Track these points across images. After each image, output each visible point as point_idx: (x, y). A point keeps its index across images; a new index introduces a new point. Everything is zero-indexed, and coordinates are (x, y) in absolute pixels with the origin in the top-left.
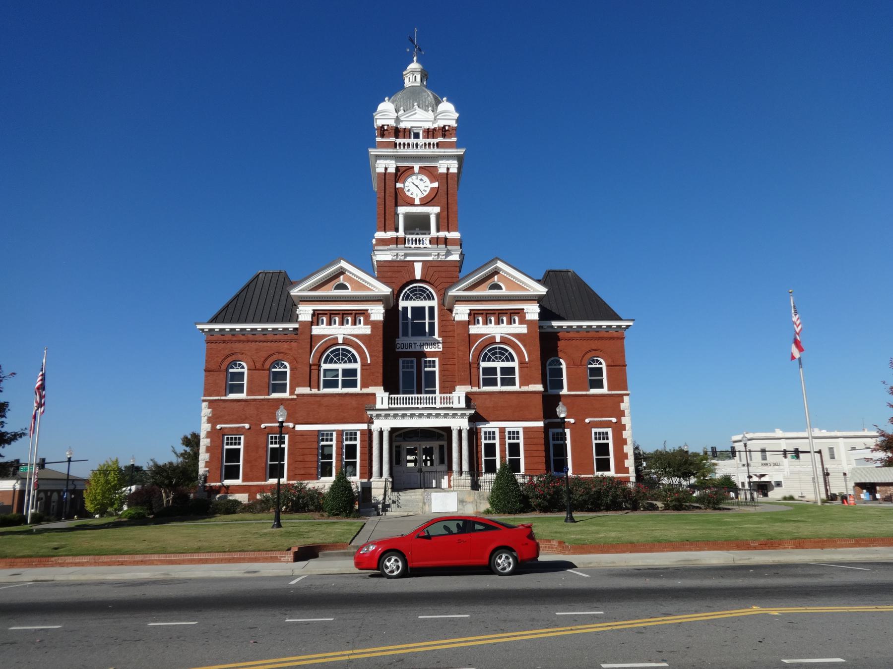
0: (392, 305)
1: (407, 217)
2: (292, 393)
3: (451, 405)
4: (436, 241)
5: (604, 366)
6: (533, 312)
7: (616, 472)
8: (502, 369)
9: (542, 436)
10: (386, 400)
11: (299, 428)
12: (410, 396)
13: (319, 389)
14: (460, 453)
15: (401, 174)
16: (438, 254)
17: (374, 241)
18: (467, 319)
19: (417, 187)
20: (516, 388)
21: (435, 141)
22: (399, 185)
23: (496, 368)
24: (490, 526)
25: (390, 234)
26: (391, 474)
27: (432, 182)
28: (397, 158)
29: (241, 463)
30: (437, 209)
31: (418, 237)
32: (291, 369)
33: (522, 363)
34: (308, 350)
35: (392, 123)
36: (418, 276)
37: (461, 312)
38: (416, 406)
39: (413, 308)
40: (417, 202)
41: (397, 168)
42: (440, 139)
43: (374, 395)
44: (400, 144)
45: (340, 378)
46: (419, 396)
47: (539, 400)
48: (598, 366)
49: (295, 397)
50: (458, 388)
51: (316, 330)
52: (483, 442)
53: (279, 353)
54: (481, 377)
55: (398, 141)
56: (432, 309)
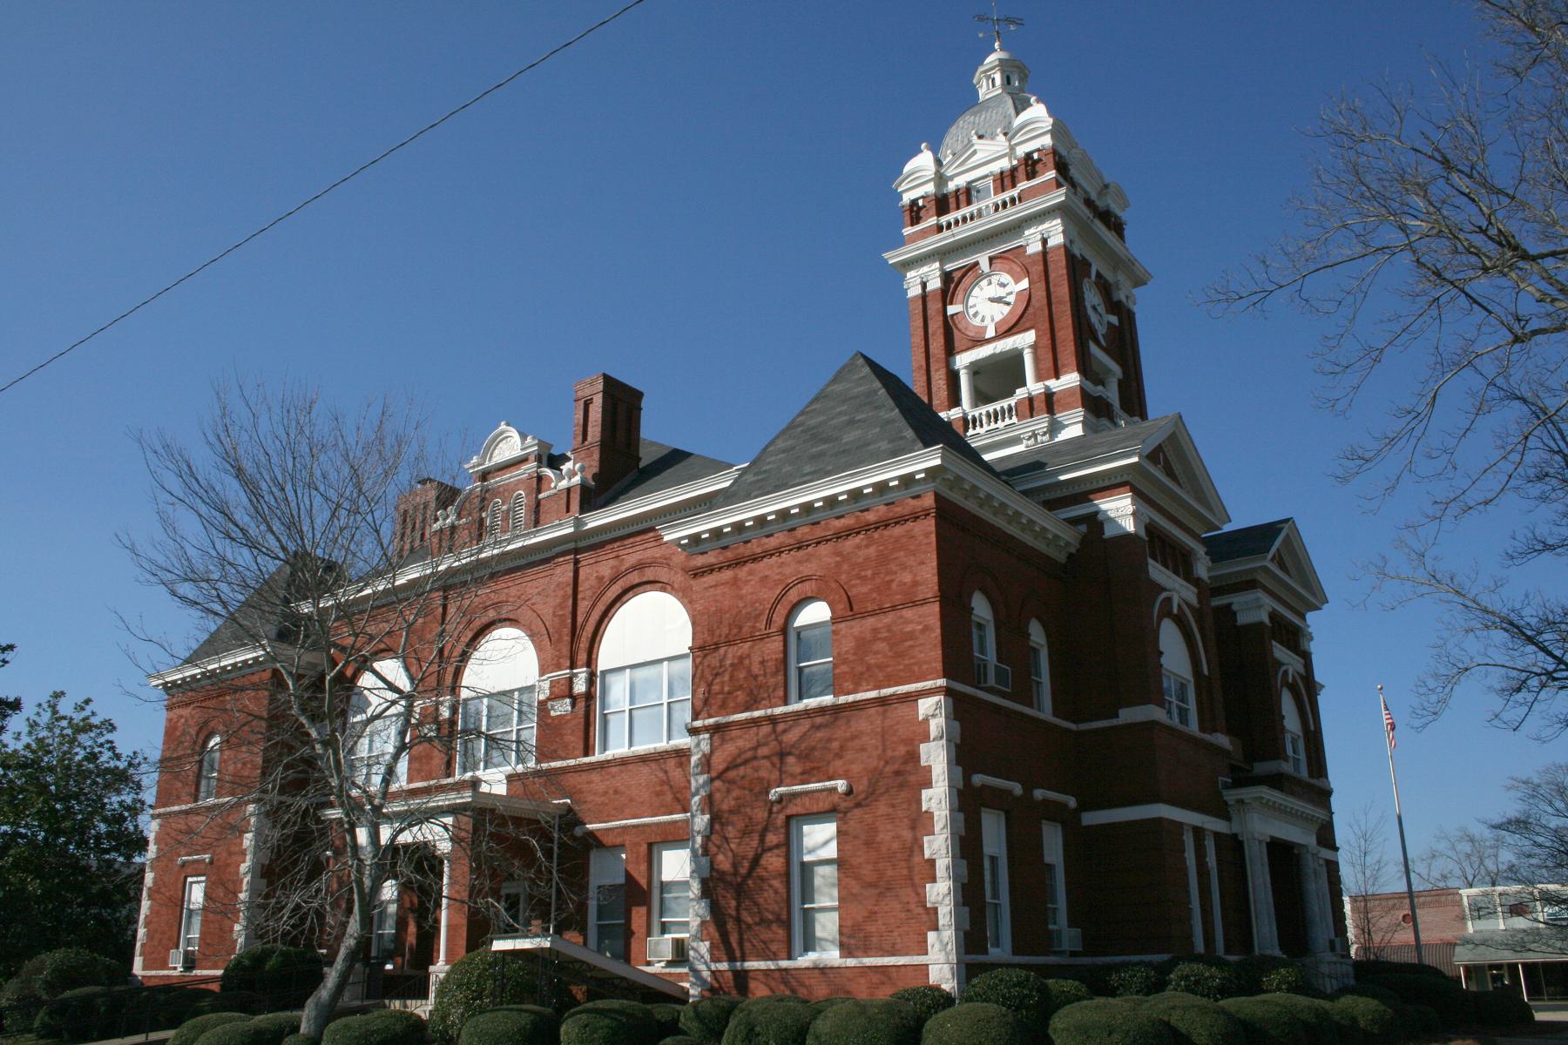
1: (976, 369)
4: (1030, 407)
15: (951, 286)
22: (951, 310)
24: (408, 978)
27: (1017, 281)
55: (944, 220)
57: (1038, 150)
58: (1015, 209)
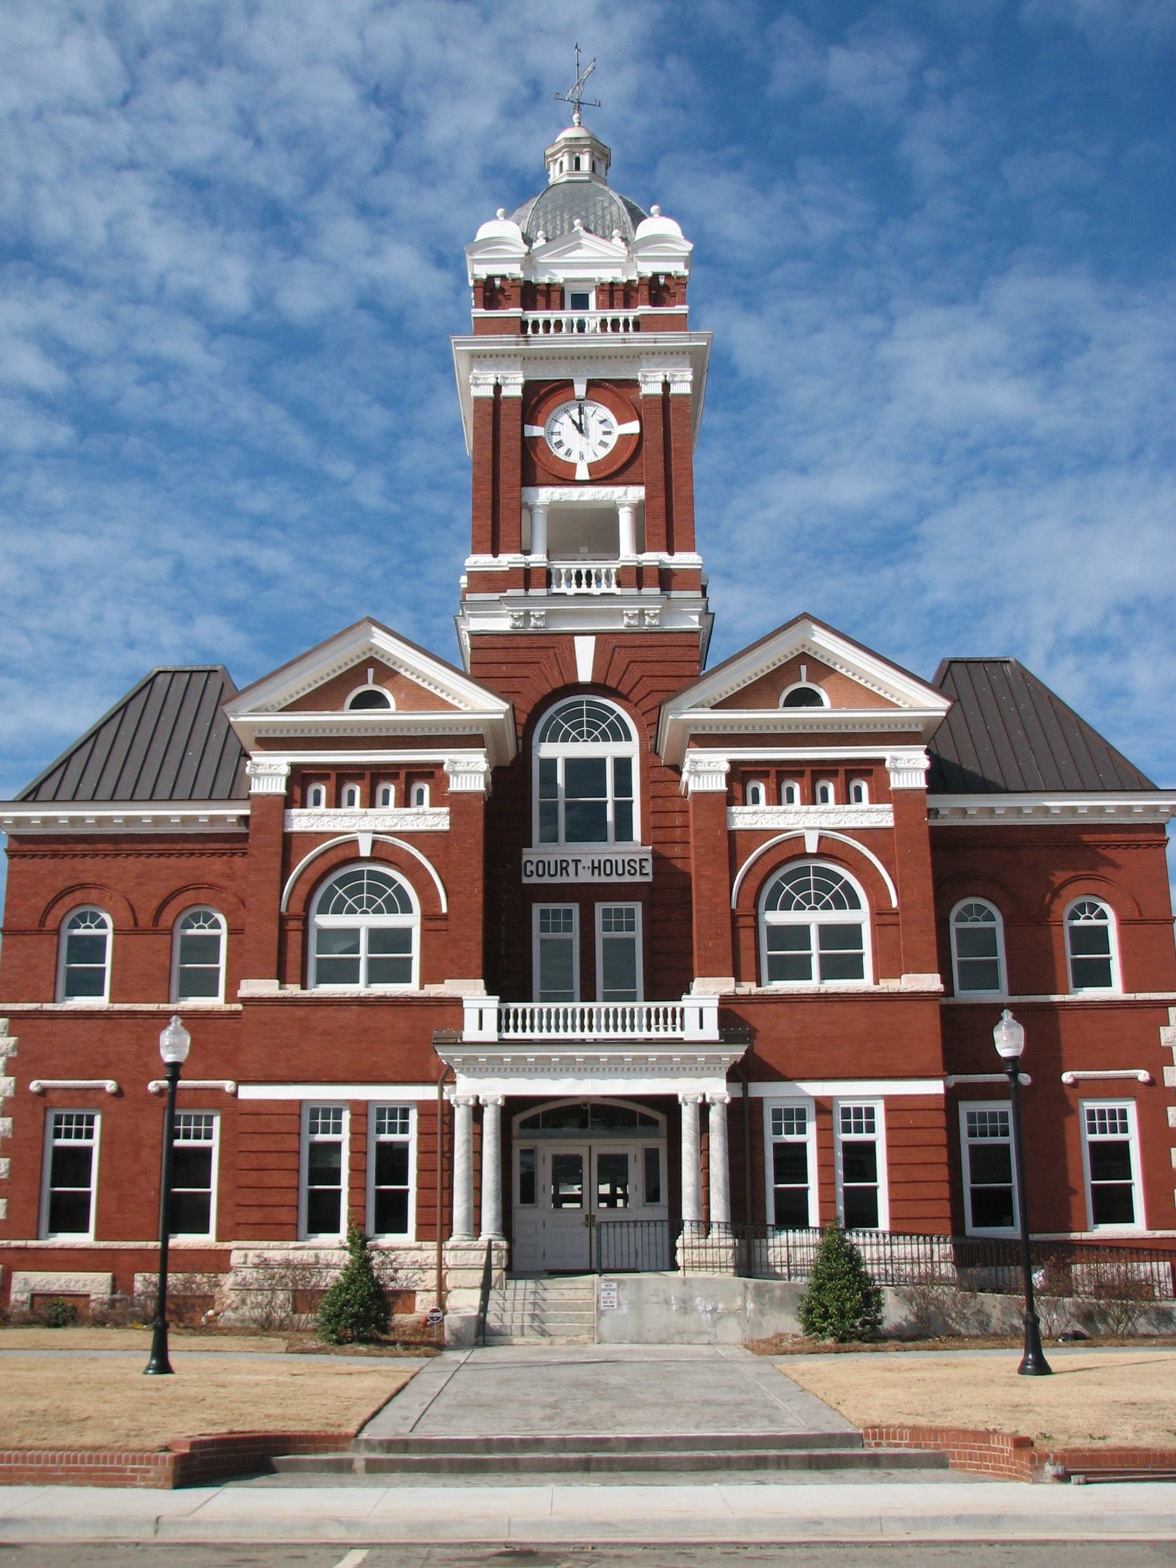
0: (511, 752)
1: (556, 512)
2: (231, 997)
3: (678, 1034)
5: (1112, 923)
6: (909, 767)
7: (1151, 1226)
8: (824, 929)
9: (941, 1119)
10: (491, 1019)
11: (248, 1093)
12: (562, 1006)
13: (304, 987)
14: (704, 1172)
15: (541, 397)
16: (642, 614)
17: (464, 579)
18: (722, 786)
19: (584, 436)
20: (866, 983)
21: (631, 314)
23: (806, 928)
25: (507, 561)
26: (506, 1227)
28: (526, 359)
29: (93, 1188)
30: (637, 493)
31: (584, 567)
32: (231, 932)
33: (880, 913)
34: (276, 875)
35: (515, 271)
36: (585, 674)
37: (706, 771)
38: (578, 1035)
39: (569, 762)
40: (582, 474)
41: (528, 386)
42: (644, 309)
43: (457, 1002)
44: (547, 324)
45: (363, 954)
46: (587, 1005)
47: (929, 1022)
48: (1094, 922)
49: (238, 1007)
50: (698, 984)
51: (301, 821)
52: (770, 1140)
53: (198, 886)
54: (765, 952)
55: (531, 316)
56: (623, 765)
57: (503, 278)
58: (616, 336)
